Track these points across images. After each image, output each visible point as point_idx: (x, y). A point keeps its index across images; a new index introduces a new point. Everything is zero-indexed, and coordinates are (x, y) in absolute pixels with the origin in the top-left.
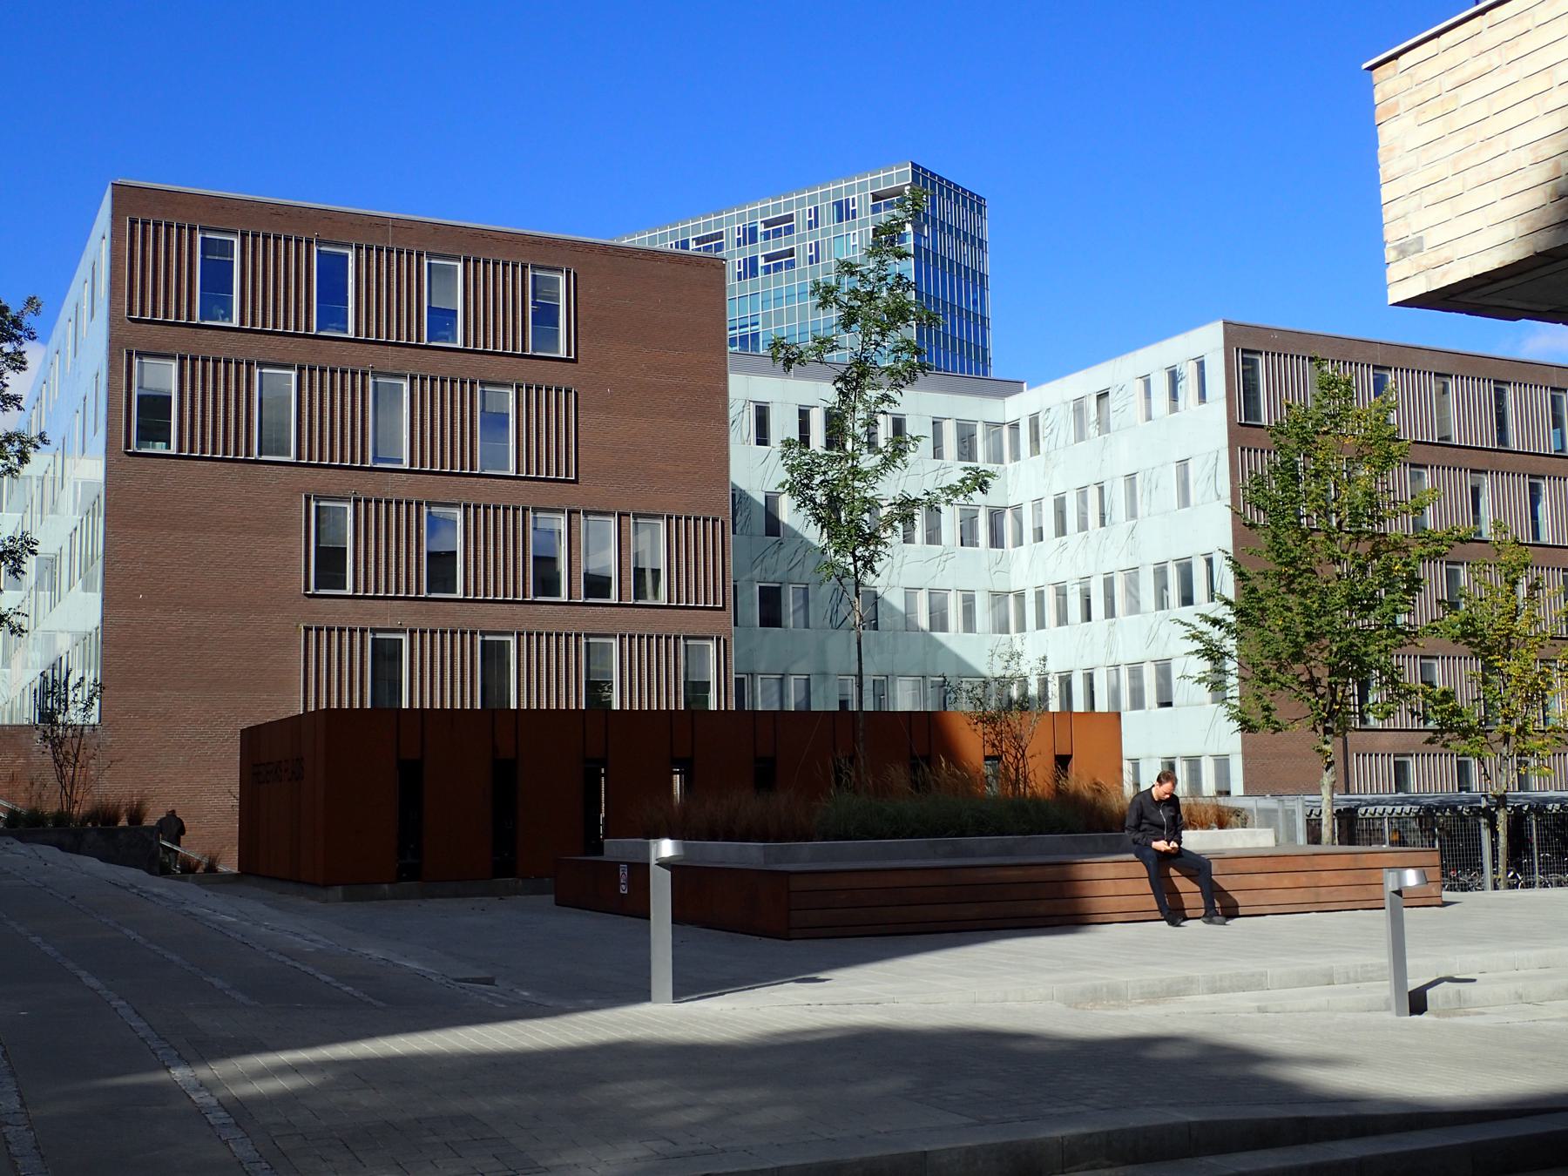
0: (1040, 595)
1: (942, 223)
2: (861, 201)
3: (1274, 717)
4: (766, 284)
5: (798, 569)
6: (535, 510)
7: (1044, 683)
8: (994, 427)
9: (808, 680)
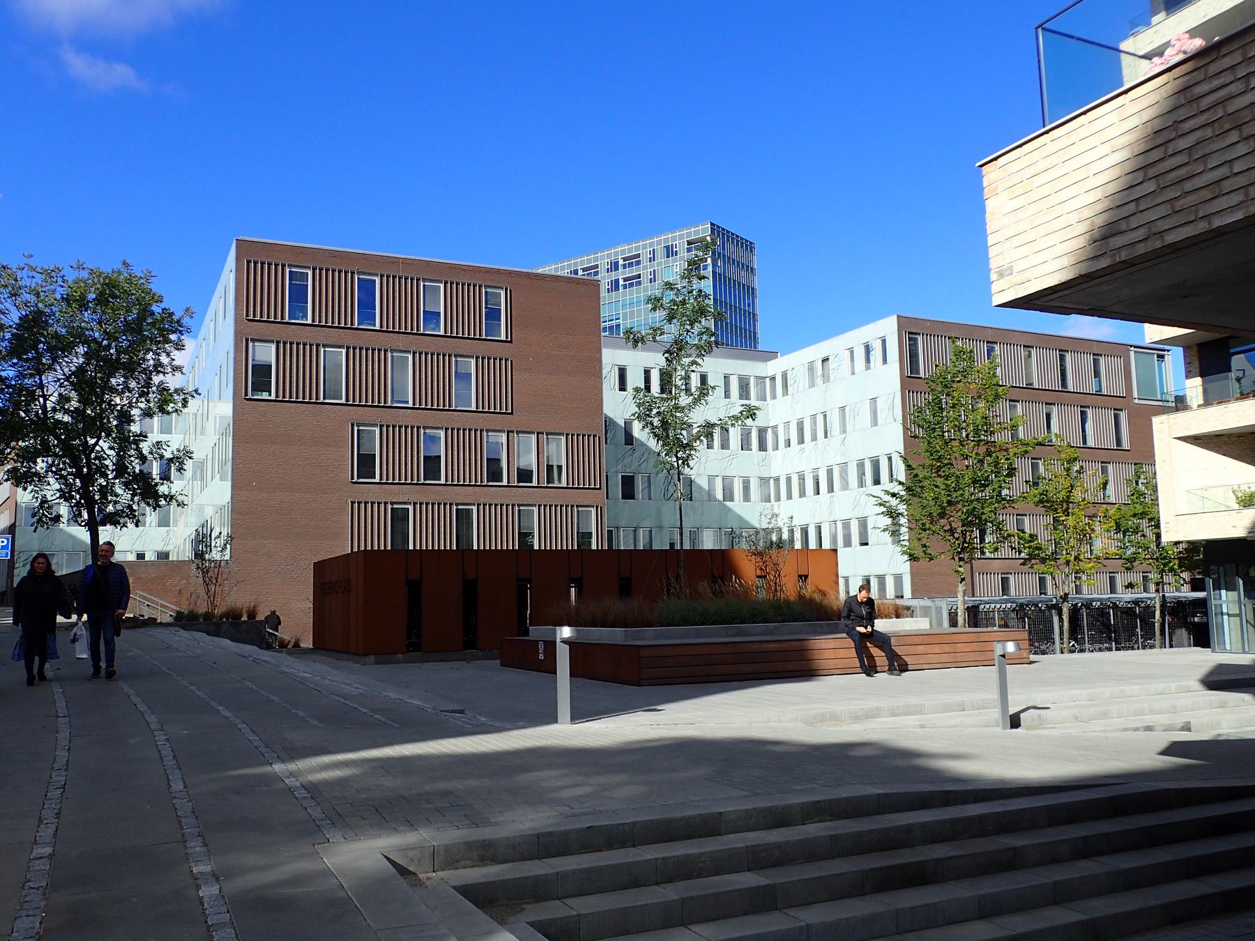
0: (789, 480)
6: (488, 431)
7: (792, 532)
8: (761, 379)
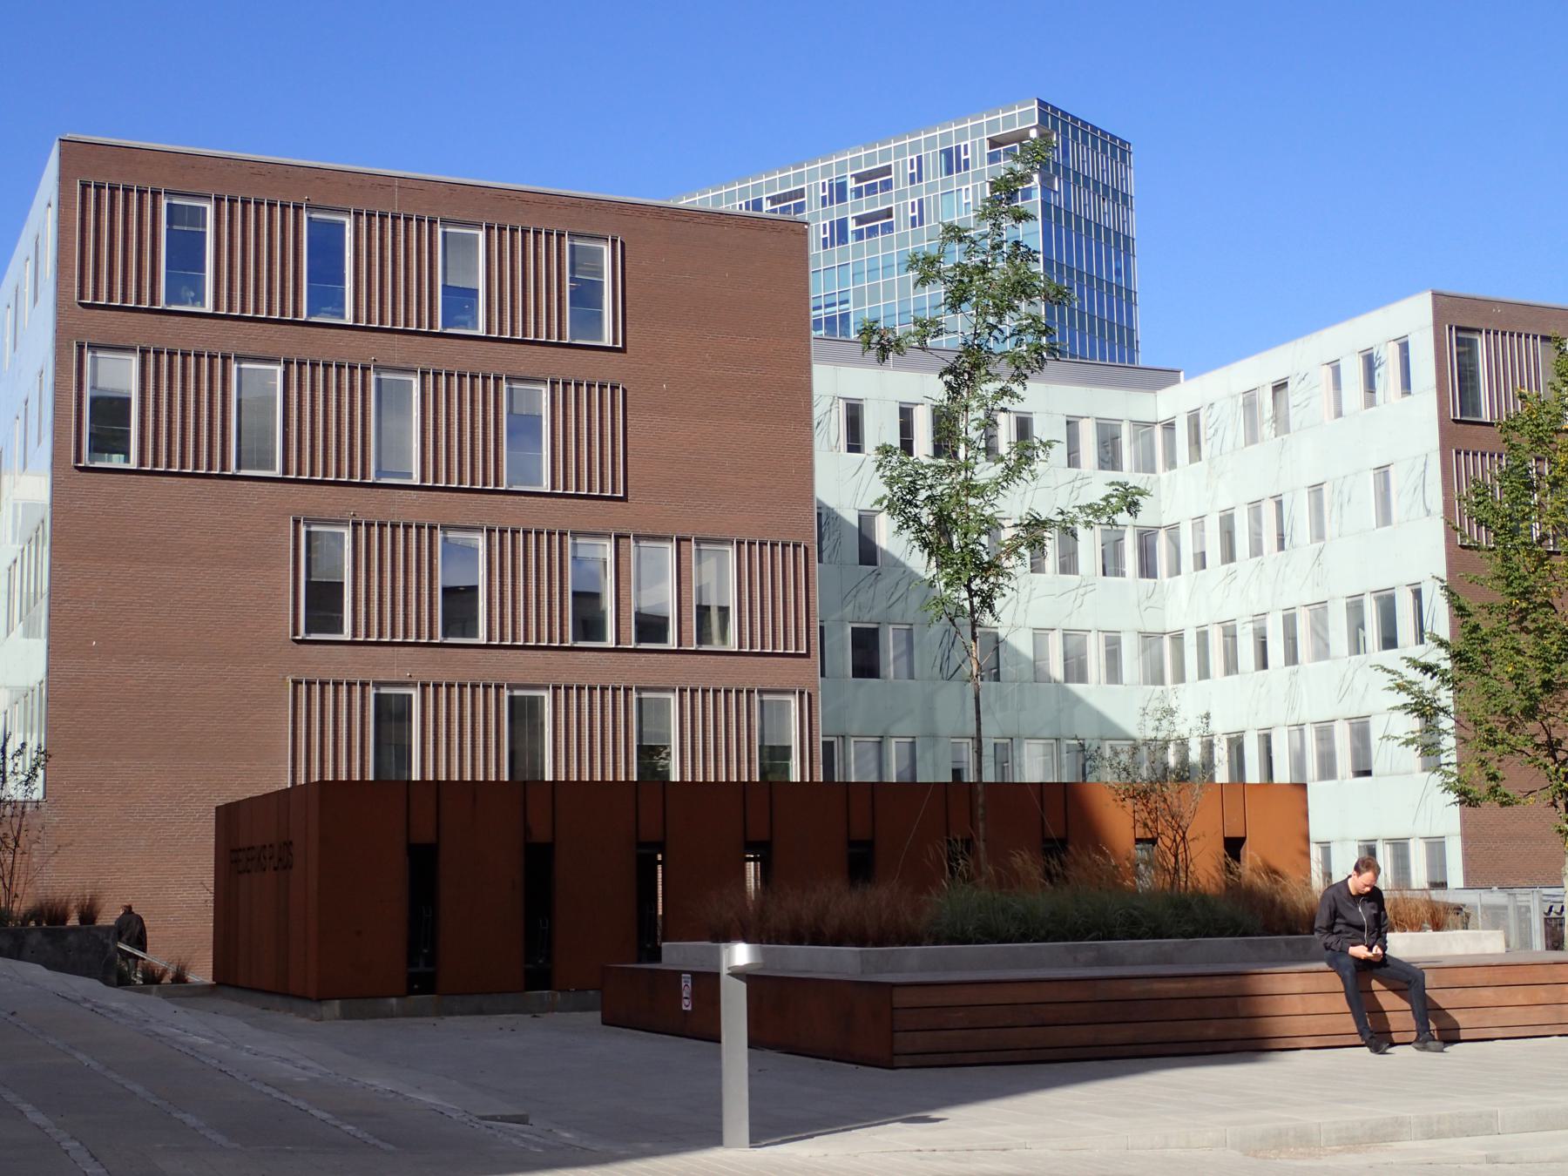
0: (1203, 637)
1: (1076, 174)
2: (975, 148)
3: (1503, 789)
4: (858, 252)
5: (898, 609)
6: (575, 534)
7: (1209, 747)
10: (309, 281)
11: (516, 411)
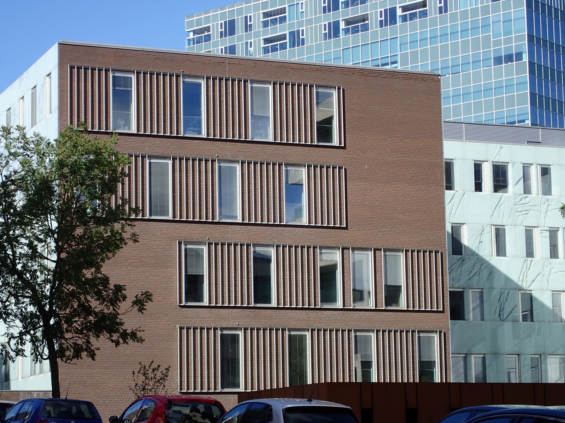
4: (403, 30)
5: (476, 278)
6: (321, 248)
9: (484, 358)
10: (184, 115)
11: (290, 182)
